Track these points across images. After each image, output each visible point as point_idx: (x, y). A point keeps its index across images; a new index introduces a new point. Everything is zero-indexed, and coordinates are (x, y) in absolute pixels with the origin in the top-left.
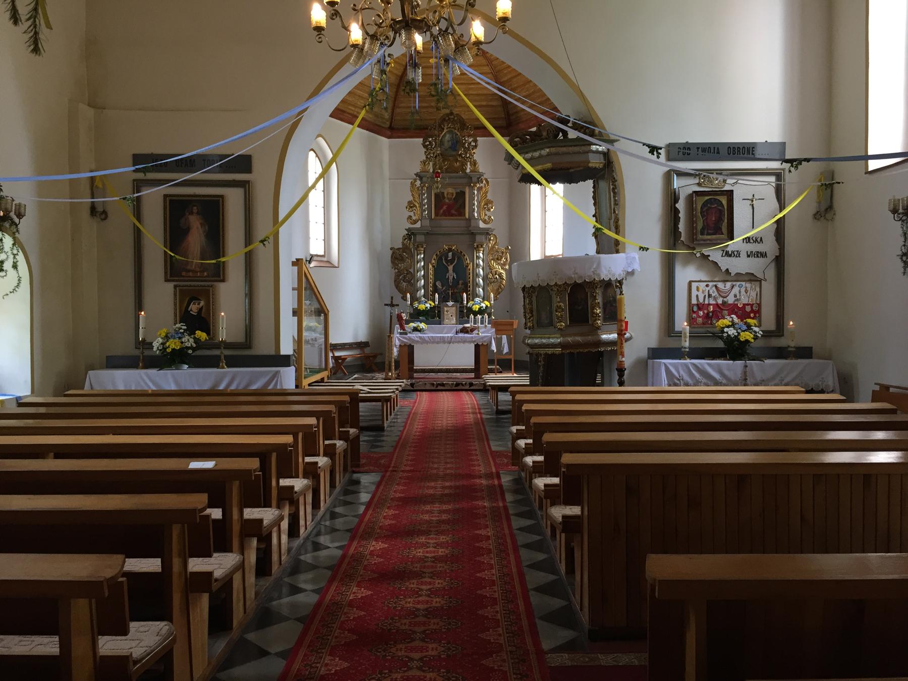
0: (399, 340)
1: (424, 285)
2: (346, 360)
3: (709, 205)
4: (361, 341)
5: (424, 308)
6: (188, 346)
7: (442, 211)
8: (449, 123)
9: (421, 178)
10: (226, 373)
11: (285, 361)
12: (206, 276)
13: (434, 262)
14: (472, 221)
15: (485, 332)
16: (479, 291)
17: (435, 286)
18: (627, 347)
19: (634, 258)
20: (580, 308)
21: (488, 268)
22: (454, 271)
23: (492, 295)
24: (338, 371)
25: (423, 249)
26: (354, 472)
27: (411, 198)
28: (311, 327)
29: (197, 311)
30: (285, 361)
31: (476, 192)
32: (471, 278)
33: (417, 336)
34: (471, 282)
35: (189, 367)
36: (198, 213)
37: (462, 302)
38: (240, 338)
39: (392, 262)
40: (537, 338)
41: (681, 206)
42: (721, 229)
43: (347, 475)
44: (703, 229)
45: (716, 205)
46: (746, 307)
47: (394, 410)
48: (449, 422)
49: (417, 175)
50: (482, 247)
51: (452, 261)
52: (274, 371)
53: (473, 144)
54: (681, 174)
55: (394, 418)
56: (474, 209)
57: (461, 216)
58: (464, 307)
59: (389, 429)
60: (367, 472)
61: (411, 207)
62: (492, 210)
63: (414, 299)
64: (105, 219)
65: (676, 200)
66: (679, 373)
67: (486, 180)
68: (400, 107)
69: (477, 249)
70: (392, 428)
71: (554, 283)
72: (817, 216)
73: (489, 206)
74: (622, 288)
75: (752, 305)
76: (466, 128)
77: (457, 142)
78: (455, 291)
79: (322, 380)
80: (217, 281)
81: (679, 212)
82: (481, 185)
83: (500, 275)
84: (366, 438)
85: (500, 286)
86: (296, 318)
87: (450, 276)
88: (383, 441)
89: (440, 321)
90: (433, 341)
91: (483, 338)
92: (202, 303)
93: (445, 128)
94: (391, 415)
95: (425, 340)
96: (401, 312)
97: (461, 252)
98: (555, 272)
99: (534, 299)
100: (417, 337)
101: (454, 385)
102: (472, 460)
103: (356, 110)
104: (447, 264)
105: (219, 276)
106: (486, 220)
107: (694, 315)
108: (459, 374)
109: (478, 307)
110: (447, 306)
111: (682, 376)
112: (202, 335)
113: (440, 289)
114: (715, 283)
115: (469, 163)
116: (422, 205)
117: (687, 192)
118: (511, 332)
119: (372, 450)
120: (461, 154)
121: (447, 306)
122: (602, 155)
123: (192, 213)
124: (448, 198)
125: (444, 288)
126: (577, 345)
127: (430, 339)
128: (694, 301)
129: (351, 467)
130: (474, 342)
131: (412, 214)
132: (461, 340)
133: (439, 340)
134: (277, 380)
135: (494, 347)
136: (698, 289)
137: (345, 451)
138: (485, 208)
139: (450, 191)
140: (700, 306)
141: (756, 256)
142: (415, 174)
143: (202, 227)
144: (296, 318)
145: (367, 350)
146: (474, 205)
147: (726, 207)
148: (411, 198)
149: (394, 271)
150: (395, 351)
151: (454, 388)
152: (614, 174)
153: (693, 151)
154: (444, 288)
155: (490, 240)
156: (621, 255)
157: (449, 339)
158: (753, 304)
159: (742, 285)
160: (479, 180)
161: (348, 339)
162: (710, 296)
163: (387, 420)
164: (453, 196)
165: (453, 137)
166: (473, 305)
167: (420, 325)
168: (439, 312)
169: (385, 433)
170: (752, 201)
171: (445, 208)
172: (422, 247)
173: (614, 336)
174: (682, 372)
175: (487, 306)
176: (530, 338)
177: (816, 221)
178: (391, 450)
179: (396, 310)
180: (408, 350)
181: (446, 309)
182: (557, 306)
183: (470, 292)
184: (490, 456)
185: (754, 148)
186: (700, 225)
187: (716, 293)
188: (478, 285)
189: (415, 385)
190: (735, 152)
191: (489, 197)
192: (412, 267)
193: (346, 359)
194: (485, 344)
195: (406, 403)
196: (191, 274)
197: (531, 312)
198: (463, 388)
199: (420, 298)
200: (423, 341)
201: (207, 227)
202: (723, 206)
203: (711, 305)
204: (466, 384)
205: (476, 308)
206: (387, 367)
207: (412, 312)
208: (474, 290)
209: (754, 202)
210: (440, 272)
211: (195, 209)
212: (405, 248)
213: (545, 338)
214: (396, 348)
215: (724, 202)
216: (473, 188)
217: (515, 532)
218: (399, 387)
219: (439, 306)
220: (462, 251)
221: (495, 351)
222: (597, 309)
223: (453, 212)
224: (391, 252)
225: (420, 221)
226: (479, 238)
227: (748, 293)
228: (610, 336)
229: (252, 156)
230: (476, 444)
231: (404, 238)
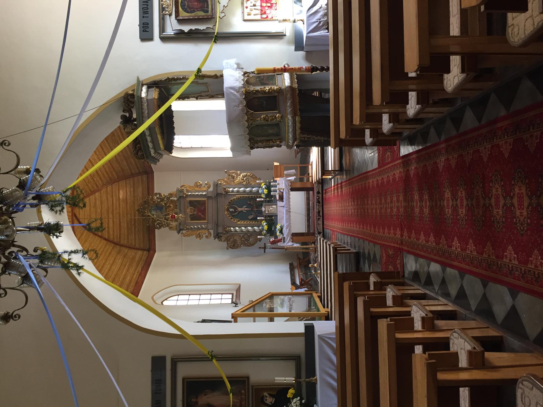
0: (288, 242)
1: (251, 227)
2: (302, 278)
3: (186, 7)
4: (290, 268)
6: (299, 403)
7: (202, 216)
8: (145, 212)
9: (181, 230)
10: (321, 378)
11: (310, 329)
12: (245, 391)
13: (235, 221)
15: (281, 183)
17: (252, 220)
18: (294, 65)
19: (227, 63)
20: (265, 102)
21: (240, 185)
22: (242, 208)
23: (257, 181)
24: (310, 284)
25: (227, 228)
26: (404, 276)
27: (194, 236)
28: (281, 303)
29: (272, 398)
30: (310, 329)
31: (189, 193)
32: (246, 196)
33: (285, 230)
34: (249, 196)
35: (316, 404)
36: (197, 398)
37: (262, 201)
38: (291, 365)
40: (288, 136)
41: (186, 28)
43: (408, 281)
47: (340, 245)
48: (350, 204)
49: (179, 233)
50: (225, 189)
51: (235, 209)
52: (318, 340)
53: (158, 196)
54: (162, 28)
55: (347, 245)
56: (201, 194)
57: (205, 203)
58: (265, 200)
59: (357, 248)
60: (403, 266)
61: (200, 236)
62: (201, 183)
63: (260, 233)
65: (181, 32)
66: (315, 22)
67: (181, 187)
68: (135, 245)
69: (227, 192)
70: (356, 245)
71: (246, 122)
74: (249, 72)
76: (147, 201)
77: (157, 206)
78: (255, 206)
79: (320, 297)
80: (248, 382)
81: (191, 29)
83: (244, 177)
84: (367, 265)
85: (251, 177)
86: (275, 318)
87: (246, 210)
88: (369, 253)
89: (275, 216)
90: (289, 219)
91: (286, 186)
92: (266, 394)
93: (148, 214)
94: (345, 247)
95: (288, 225)
96: (270, 241)
97: (229, 203)
98: (238, 122)
99: (259, 139)
100: (286, 231)
102: (388, 181)
103: (136, 273)
104: (237, 212)
105: (245, 381)
106: (208, 187)
108: (310, 202)
109: (265, 190)
110: (265, 211)
111: (317, 19)
112: (291, 391)
113: (254, 216)
115: (171, 199)
116: (198, 229)
118: (282, 166)
119: (378, 261)
120: (165, 204)
121: (265, 211)
122: (150, 90)
123: (197, 403)
124: (194, 212)
125: (253, 214)
126: (293, 104)
128: (259, 17)
129: (400, 279)
130: (289, 192)
131: (204, 236)
132: (288, 201)
134: (325, 337)
135: (292, 178)
136: (249, 15)
137: (396, 284)
142: (178, 234)
144: (275, 318)
145: (295, 264)
146: (198, 195)
148: (194, 236)
149: (242, 247)
150: (296, 245)
152: (163, 80)
153: (145, 20)
154: (253, 214)
155: (221, 184)
156: (226, 73)
161: (287, 278)
162: (254, 5)
163: (349, 250)
164: (192, 209)
165: (153, 209)
166: (264, 194)
167: (278, 228)
168: (269, 216)
169: (361, 251)
171: (200, 214)
173: (287, 75)
174: (314, 20)
175: (264, 185)
176: (288, 142)
179: (268, 245)
180: (295, 236)
181: (267, 212)
182: (264, 120)
183: (255, 196)
184: (382, 169)
186: (201, 14)
188: (251, 191)
192: (240, 235)
193: (301, 278)
194: (290, 184)
195: (333, 237)
196: (243, 403)
197: (268, 141)
198: (321, 198)
199: (260, 229)
200: (289, 226)
201: (208, 391)
203: (261, 4)
204: (318, 196)
205: (266, 191)
206: (307, 251)
207: (269, 235)
208: (254, 193)
210: (242, 216)
211: (194, 400)
212: (227, 240)
213: (288, 130)
216: (187, 196)
217: (483, 122)
218: (324, 242)
219: (265, 216)
220: (228, 202)
221: (295, 177)
222: (265, 89)
223: (203, 208)
224: (230, 249)
225: (209, 230)
226: (220, 191)
228: (286, 80)
229: (152, 356)
230: (371, 181)
231: (220, 240)
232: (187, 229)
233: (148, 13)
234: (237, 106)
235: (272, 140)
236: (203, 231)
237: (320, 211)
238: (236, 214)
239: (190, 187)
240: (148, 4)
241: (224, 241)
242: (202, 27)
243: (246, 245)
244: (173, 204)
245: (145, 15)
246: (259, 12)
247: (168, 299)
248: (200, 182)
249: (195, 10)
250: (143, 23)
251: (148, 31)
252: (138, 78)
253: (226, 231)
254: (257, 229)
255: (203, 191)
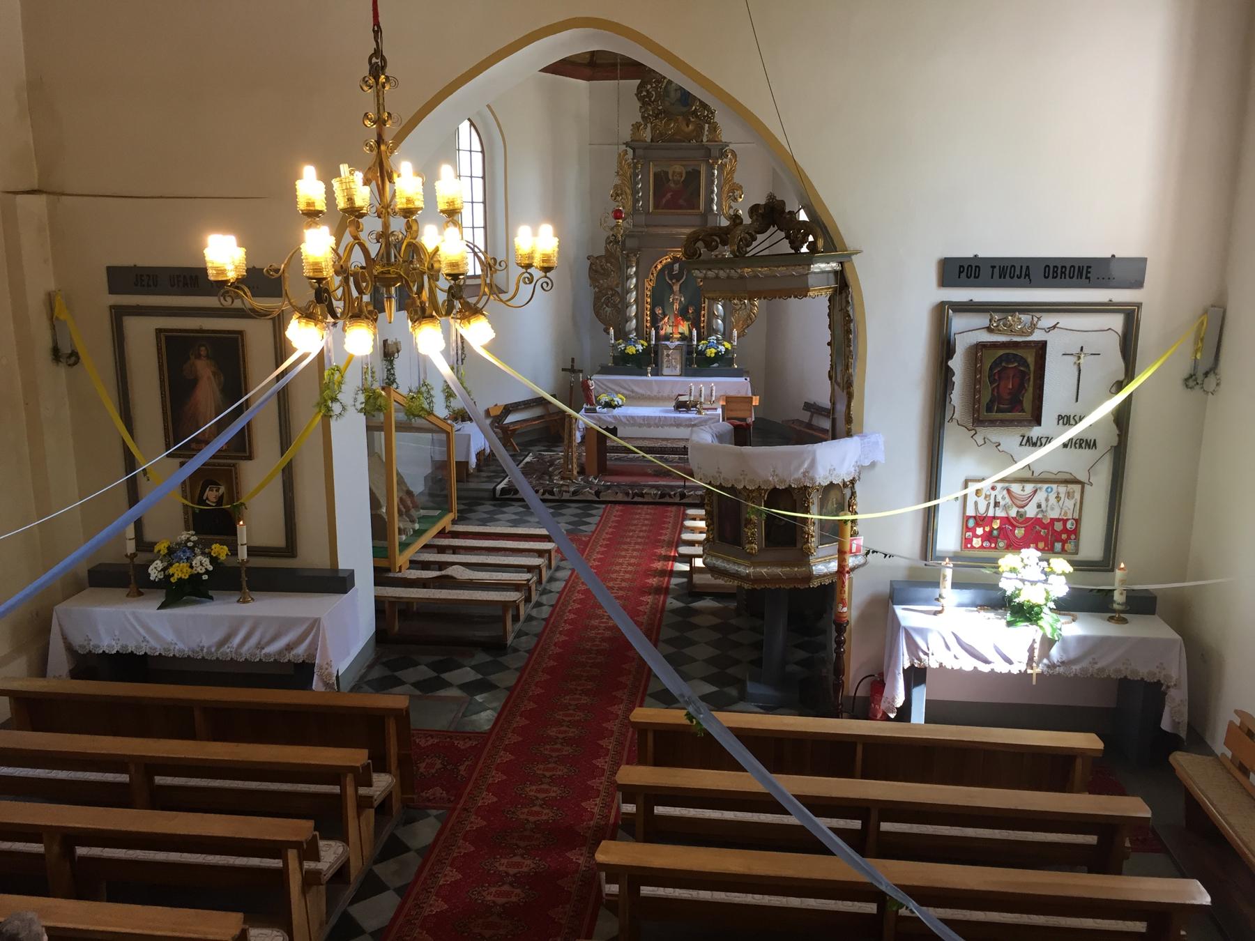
2: (517, 432)
5: (635, 352)
7: (664, 201)
14: (709, 217)
16: (717, 323)
23: (735, 333)
27: (617, 181)
31: (716, 172)
36: (208, 357)
39: (590, 277)
41: (957, 363)
42: (1021, 402)
44: (992, 402)
45: (1016, 364)
46: (1056, 523)
56: (713, 199)
57: (693, 209)
61: (617, 195)
62: (741, 200)
64: (76, 363)
67: (733, 152)
72: (1191, 381)
73: (736, 194)
74: (853, 487)
75: (1065, 521)
82: (725, 160)
85: (749, 316)
92: (222, 489)
95: (621, 420)
98: (743, 471)
100: (609, 416)
101: (658, 496)
107: (969, 534)
109: (714, 351)
112: (220, 550)
114: (1006, 485)
116: (635, 192)
117: (968, 341)
123: (199, 356)
127: (628, 420)
133: (642, 422)
138: (730, 196)
139: (677, 170)
140: (981, 520)
141: (1077, 446)
143: (214, 376)
146: (712, 192)
147: (1032, 368)
148: (617, 181)
151: (657, 500)
153: (986, 271)
157: (657, 421)
158: (1068, 520)
159: (1052, 489)
160: (723, 155)
162: (997, 504)
164: (682, 177)
170: (1079, 358)
171: (669, 195)
172: (635, 255)
175: (727, 349)
177: (1189, 390)
178: (590, 534)
185: (1090, 267)
186: (986, 397)
187: (1008, 500)
189: (601, 494)
190: (1057, 274)
191: (737, 180)
192: (620, 286)
202: (1028, 366)
203: (998, 518)
204: (675, 494)
205: (711, 352)
209: (1082, 361)
211: (203, 351)
212: (609, 256)
214: (580, 431)
215: (1031, 360)
223: (681, 202)
227: (1061, 502)
228: (823, 565)
232: (635, 167)
233: (1000, 277)
234: (774, 471)
235: (713, 524)
236: (630, 203)
237: (644, 497)
238: (667, 278)
239: (732, 171)
240: (1023, 276)
241: (607, 250)
242: (957, 396)
243: (597, 299)
244: (693, 131)
245: (997, 271)
246: (982, 510)
247: (472, 128)
248: (741, 198)
249: (996, 384)
250: (979, 267)
251: (959, 277)
252: (857, 253)
253: (628, 256)
254: (630, 326)
255: (719, 205)
